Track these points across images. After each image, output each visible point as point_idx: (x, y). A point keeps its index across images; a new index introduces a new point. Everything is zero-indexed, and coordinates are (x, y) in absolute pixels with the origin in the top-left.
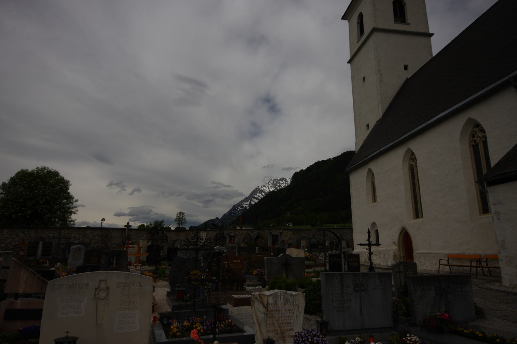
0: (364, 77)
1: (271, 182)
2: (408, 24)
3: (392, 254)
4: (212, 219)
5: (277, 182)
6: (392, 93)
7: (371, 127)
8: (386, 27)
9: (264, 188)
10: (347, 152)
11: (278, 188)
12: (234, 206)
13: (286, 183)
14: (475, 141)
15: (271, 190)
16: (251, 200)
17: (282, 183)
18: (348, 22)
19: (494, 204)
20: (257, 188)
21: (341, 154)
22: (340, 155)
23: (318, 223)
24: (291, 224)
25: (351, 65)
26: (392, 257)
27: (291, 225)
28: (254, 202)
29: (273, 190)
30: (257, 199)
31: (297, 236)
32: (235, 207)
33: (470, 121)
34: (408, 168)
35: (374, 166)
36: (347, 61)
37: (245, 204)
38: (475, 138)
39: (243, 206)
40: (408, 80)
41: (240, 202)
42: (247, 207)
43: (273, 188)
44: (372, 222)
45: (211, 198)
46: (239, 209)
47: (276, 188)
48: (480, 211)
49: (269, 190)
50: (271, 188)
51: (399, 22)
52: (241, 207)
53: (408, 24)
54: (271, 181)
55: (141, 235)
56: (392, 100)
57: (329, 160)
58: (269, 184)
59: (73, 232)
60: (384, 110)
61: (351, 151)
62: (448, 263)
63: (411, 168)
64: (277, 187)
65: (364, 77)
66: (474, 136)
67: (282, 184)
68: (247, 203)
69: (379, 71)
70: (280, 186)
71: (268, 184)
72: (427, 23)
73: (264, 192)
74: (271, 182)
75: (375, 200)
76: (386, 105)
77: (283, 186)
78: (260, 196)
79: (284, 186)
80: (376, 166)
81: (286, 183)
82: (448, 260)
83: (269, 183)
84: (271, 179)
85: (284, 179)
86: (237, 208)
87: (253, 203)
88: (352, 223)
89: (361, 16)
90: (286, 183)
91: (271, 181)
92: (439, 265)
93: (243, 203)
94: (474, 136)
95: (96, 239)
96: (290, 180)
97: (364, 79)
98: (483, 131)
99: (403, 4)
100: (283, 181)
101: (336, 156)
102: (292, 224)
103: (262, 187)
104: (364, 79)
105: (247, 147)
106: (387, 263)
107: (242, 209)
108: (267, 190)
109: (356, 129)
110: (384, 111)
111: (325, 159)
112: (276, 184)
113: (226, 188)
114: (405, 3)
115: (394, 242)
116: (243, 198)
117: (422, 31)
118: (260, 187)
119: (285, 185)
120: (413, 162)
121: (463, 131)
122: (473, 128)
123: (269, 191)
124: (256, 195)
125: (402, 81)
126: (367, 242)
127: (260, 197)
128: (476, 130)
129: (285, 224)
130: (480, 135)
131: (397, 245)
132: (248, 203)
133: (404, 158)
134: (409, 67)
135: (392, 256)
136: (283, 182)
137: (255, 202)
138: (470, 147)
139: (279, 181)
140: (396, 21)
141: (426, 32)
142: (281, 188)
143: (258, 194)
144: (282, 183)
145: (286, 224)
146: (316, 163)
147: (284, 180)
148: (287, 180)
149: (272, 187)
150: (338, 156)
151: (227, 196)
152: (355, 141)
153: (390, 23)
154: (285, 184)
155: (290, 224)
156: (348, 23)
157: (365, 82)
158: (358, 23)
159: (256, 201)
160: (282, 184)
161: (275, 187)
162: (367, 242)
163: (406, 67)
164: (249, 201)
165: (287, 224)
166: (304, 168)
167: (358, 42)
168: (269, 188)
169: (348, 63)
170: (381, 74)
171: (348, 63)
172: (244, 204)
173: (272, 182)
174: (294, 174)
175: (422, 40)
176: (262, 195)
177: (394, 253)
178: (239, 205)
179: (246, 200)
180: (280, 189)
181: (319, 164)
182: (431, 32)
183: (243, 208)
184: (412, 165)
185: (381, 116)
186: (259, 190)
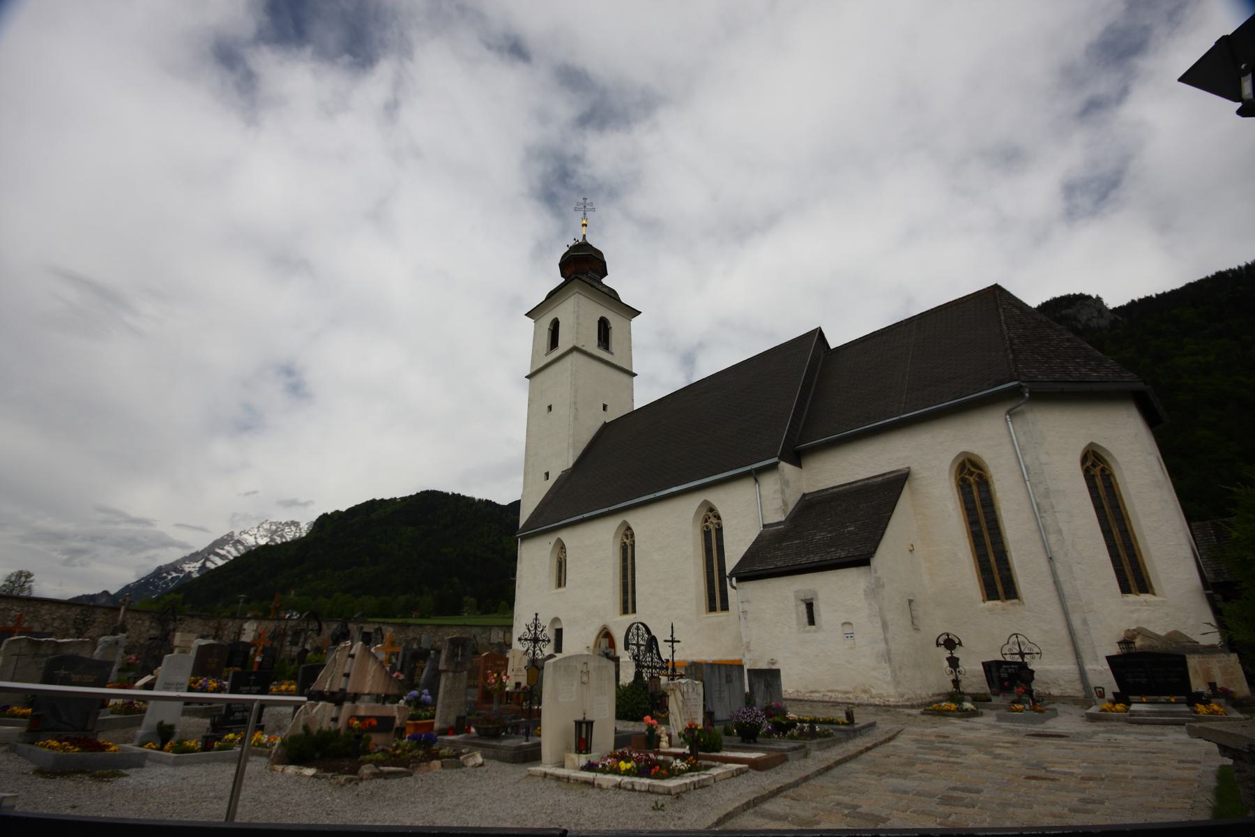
0: (551, 406)
2: (612, 354)
4: (91, 594)
5: (278, 528)
6: (587, 437)
9: (245, 536)
10: (427, 491)
11: (279, 541)
12: (160, 568)
13: (298, 531)
14: (707, 527)
16: (207, 559)
17: (289, 530)
19: (742, 602)
20: (228, 535)
21: (418, 494)
22: (415, 495)
23: (356, 616)
28: (213, 562)
29: (267, 544)
30: (222, 557)
31: (401, 636)
32: (159, 572)
33: (706, 503)
34: (619, 545)
35: (567, 536)
36: (526, 375)
37: (190, 565)
38: (707, 524)
39: (182, 571)
41: (178, 561)
42: (192, 573)
44: (554, 616)
45: (83, 545)
46: (171, 575)
47: (272, 540)
48: (706, 609)
49: (256, 542)
52: (176, 572)
53: (612, 354)
55: (139, 622)
57: (393, 500)
58: (258, 531)
59: (15, 607)
60: (575, 459)
61: (434, 491)
63: (623, 547)
64: (276, 537)
65: (551, 406)
66: (706, 521)
68: (195, 564)
69: (575, 403)
70: (282, 536)
72: (631, 359)
73: (242, 544)
75: (561, 582)
76: (579, 452)
77: (289, 538)
78: (232, 552)
80: (574, 539)
83: (259, 527)
84: (267, 520)
85: (295, 524)
86: (166, 573)
87: (210, 565)
88: (512, 617)
93: (186, 564)
94: (706, 521)
95: (55, 625)
96: (307, 526)
97: (550, 408)
98: (719, 518)
101: (408, 495)
104: (550, 408)
105: (222, 449)
107: (178, 576)
108: (250, 541)
111: (387, 498)
112: (276, 531)
113: (136, 528)
115: (588, 647)
116: (187, 553)
117: (626, 367)
118: (236, 534)
119: (295, 536)
120: (627, 539)
121: (697, 513)
122: (707, 512)
123: (254, 544)
124: (223, 549)
125: (599, 425)
126: (671, 639)
127: (231, 555)
128: (710, 514)
129: (283, 615)
130: (715, 521)
132: (198, 565)
133: (616, 533)
134: (608, 408)
137: (216, 564)
141: (630, 369)
143: (227, 548)
144: (289, 530)
145: (286, 613)
146: (367, 502)
147: (295, 526)
150: (411, 496)
151: (132, 544)
152: (522, 491)
153: (592, 345)
156: (533, 324)
158: (549, 329)
159: (220, 562)
162: (671, 639)
163: (605, 407)
164: (202, 561)
165: (288, 615)
166: (343, 509)
167: (546, 355)
168: (256, 538)
170: (576, 409)
172: (187, 566)
173: (266, 526)
174: (320, 517)
175: (625, 377)
176: (237, 550)
178: (174, 567)
179: (193, 557)
180: (283, 543)
181: (372, 506)
182: (634, 371)
183: (181, 573)
184: (625, 543)
185: (570, 465)
186: (232, 540)
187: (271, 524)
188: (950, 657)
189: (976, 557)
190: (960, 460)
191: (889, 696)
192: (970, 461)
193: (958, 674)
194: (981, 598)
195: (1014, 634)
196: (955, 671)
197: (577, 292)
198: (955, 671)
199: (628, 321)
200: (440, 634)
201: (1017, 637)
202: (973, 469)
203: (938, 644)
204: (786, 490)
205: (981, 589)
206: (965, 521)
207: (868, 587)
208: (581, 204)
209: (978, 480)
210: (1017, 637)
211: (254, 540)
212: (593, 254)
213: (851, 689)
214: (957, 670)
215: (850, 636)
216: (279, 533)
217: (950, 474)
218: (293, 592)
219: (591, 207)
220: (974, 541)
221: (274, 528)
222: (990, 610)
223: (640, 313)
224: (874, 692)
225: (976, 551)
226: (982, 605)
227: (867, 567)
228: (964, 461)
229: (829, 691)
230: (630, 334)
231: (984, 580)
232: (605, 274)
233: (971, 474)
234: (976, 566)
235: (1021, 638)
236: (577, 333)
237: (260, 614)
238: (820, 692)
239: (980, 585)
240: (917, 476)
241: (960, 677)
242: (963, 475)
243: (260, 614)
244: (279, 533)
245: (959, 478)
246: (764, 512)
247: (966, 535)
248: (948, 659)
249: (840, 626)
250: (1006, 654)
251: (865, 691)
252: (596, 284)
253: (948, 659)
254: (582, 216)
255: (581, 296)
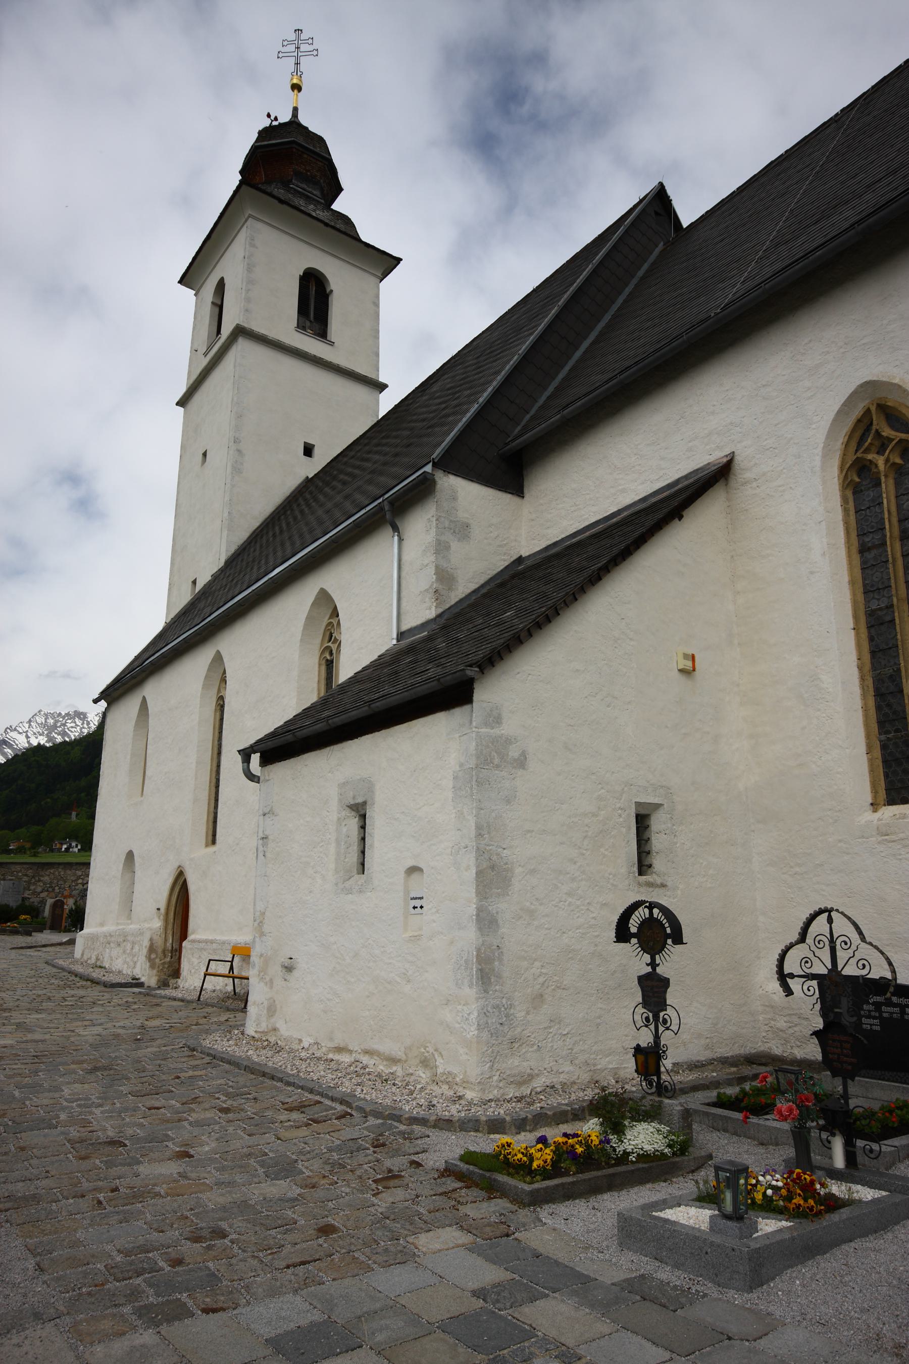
1: (39, 721)
2: (332, 344)
3: (146, 943)
5: (57, 721)
7: (200, 586)
8: (272, 334)
9: (14, 735)
11: (59, 739)
13: (85, 726)
15: (35, 743)
17: (73, 725)
18: (195, 295)
24: (77, 846)
25: (185, 413)
26: (145, 951)
27: (76, 850)
40: (308, 481)
43: (40, 738)
47: (50, 739)
49: (28, 742)
50: (37, 738)
51: (309, 331)
53: (332, 344)
54: (37, 718)
56: (258, 524)
58: (30, 726)
60: (233, 549)
62: (232, 968)
64: (56, 736)
67: (73, 730)
69: (236, 441)
70: (64, 734)
71: (26, 726)
73: (10, 746)
74: (39, 721)
76: (242, 535)
77: (74, 735)
79: (77, 734)
81: (84, 728)
82: (232, 962)
83: (30, 721)
84: (40, 711)
85: (82, 716)
88: (90, 856)
89: (221, 287)
90: (84, 728)
91: (37, 718)
92: (205, 975)
99: (328, 291)
100: (77, 720)
102: (79, 847)
103: (6, 730)
106: (134, 967)
108: (22, 742)
109: (169, 589)
110: (233, 551)
112: (55, 727)
114: (332, 291)
115: (158, 909)
123: (27, 745)
131: (162, 917)
134: (316, 451)
135: (146, 947)
136: (75, 722)
138: (320, 665)
139: (64, 718)
140: (301, 327)
141: (373, 376)
142: (67, 739)
144: (73, 725)
145: (62, 844)
147: (80, 718)
148: (89, 720)
149: (40, 735)
154: (81, 729)
155: (74, 844)
157: (206, 463)
160: (72, 727)
161: (47, 736)
163: (308, 451)
165: (65, 846)
168: (27, 737)
169: (178, 404)
171: (178, 404)
177: (151, 940)
182: (382, 379)
185: (222, 563)
187: (46, 716)
188: (648, 974)
189: (870, 682)
190: (857, 412)
191: (465, 1083)
192: (883, 408)
193: (661, 1029)
194: (867, 797)
195: (820, 912)
196: (656, 1017)
197: (250, 216)
198: (656, 1017)
199: (375, 280)
200: (46, 879)
201: (830, 920)
202: (887, 432)
203: (622, 934)
204: (455, 545)
205: (872, 770)
206: (852, 582)
207: (461, 765)
208: (291, 42)
209: (898, 461)
210: (830, 920)
211: (26, 741)
212: (300, 140)
213: (400, 1054)
214: (662, 1014)
215: (417, 904)
216: (60, 729)
217: (825, 455)
218: (74, 814)
219: (311, 48)
220: (871, 639)
221: (51, 721)
222: (883, 832)
223: (399, 260)
224: (442, 1066)
225: (874, 668)
226: (869, 817)
227: (467, 708)
228: (868, 412)
229: (366, 1052)
230: (377, 304)
231: (884, 747)
232: (337, 189)
233: (882, 445)
234: (865, 709)
235: (841, 927)
236: (248, 300)
237: (28, 845)
238: (350, 1052)
239: (871, 762)
240: (748, 475)
241: (666, 1038)
242: (859, 455)
243: (28, 845)
244: (60, 729)
245: (851, 458)
246: (404, 604)
247: (851, 623)
248: (642, 980)
249: (402, 875)
250: (792, 976)
251: (425, 1063)
252: (320, 214)
253: (642, 980)
254: (292, 68)
255: (259, 225)
